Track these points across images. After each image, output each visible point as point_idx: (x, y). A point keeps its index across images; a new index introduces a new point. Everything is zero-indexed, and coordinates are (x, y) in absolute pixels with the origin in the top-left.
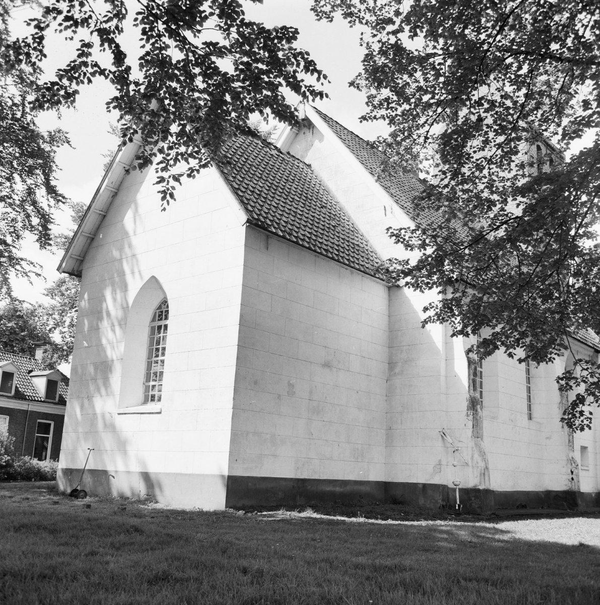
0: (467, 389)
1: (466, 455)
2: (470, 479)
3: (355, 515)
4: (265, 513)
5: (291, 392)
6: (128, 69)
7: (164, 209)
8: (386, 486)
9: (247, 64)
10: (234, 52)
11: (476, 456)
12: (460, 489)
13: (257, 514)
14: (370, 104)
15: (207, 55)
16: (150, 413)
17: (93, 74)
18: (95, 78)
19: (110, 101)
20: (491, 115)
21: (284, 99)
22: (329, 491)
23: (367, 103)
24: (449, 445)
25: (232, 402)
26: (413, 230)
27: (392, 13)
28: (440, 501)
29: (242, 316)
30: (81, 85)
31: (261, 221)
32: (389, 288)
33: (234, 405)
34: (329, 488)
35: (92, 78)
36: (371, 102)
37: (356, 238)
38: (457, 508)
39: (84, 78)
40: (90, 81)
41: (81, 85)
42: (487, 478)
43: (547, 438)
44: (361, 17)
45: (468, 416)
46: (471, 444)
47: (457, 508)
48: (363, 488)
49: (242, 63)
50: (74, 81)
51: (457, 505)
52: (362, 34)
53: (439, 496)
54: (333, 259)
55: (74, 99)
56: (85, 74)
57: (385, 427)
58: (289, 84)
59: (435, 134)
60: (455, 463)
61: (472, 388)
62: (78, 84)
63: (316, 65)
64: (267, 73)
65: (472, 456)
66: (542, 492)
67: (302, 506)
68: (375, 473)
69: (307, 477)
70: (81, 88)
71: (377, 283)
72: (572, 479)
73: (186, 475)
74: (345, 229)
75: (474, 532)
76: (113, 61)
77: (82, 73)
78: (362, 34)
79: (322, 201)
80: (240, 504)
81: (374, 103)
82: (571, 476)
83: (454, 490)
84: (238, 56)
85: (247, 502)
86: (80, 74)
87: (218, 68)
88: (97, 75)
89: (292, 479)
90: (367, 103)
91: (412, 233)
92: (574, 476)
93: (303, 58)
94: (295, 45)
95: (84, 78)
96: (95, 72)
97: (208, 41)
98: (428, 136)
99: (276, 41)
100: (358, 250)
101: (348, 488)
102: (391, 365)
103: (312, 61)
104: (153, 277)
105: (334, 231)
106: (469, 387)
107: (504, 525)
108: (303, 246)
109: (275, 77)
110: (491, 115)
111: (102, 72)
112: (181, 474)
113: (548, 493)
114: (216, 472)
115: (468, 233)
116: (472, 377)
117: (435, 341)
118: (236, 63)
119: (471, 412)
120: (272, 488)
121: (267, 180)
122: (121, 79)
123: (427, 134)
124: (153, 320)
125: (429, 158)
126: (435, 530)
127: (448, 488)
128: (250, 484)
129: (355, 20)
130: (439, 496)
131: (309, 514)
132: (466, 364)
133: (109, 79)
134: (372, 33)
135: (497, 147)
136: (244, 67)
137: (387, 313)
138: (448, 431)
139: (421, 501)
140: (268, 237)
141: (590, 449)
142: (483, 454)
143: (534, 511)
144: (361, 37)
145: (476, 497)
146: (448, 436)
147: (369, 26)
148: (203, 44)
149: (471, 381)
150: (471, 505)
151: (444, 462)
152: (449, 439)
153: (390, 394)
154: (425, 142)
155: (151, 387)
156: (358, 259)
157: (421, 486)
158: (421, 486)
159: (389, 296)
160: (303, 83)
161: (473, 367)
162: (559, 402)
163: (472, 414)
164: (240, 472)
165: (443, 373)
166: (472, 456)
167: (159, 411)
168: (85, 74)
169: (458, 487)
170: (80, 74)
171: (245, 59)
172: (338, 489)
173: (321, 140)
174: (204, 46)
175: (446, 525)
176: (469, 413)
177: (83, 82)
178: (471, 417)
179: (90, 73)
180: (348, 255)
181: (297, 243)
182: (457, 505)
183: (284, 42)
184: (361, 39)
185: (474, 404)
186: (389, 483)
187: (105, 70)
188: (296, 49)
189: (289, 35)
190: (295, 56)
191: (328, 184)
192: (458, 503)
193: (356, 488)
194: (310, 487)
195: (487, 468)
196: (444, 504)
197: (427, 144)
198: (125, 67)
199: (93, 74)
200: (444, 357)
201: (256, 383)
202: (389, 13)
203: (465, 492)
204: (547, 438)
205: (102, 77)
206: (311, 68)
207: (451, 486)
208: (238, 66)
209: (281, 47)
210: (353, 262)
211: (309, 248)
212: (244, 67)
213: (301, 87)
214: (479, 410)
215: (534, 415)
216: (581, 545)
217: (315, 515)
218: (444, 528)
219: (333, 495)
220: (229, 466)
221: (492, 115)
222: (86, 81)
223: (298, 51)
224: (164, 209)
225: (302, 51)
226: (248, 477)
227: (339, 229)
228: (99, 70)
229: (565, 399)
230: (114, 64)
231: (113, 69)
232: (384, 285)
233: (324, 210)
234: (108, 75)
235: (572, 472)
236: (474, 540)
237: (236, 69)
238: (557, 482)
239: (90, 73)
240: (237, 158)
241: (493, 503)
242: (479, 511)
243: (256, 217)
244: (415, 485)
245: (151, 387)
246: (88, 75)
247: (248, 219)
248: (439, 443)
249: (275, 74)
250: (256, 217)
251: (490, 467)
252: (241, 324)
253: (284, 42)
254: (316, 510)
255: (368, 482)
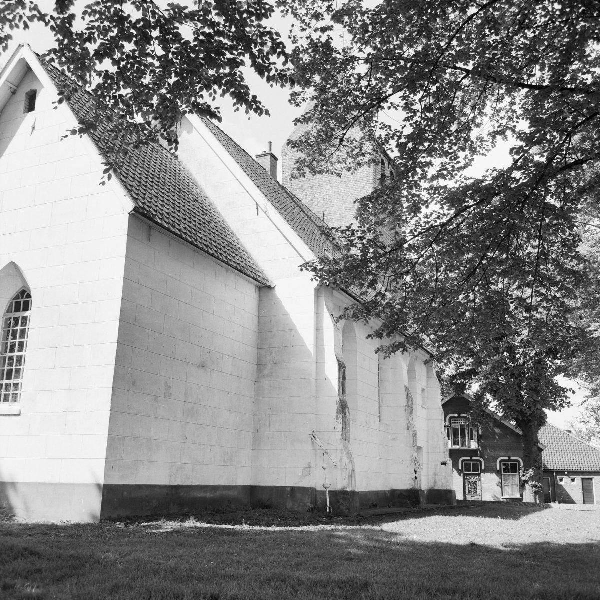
0: (338, 392)
1: (335, 457)
2: (339, 483)
3: (240, 524)
4: (145, 524)
5: (168, 395)
6: (72, 16)
7: (104, 183)
8: (252, 490)
9: (209, 36)
10: (196, 20)
11: (345, 458)
12: (330, 492)
13: (138, 525)
14: (293, 102)
15: (172, 19)
16: (9, 415)
17: (31, 18)
18: (32, 23)
19: (47, 52)
20: (411, 124)
21: (243, 79)
22: (200, 497)
23: (290, 101)
24: (319, 448)
25: (110, 404)
26: (344, 230)
27: (325, 8)
28: (309, 504)
29: (122, 311)
30: (15, 28)
31: (147, 210)
32: (260, 288)
33: (112, 407)
34: (200, 495)
35: (29, 23)
36: (294, 100)
37: (228, 235)
38: (328, 511)
39: (20, 21)
40: (26, 26)
41: (15, 28)
42: (353, 479)
43: (394, 439)
44: (295, 7)
45: (337, 418)
46: (341, 447)
47: (328, 511)
48: (231, 493)
49: (203, 33)
50: (8, 24)
51: (328, 508)
52: (293, 25)
53: (308, 499)
54: (213, 255)
55: (7, 44)
56: (21, 17)
57: (252, 430)
58: (255, 64)
59: (350, 137)
60: (325, 466)
61: (341, 391)
62: (12, 27)
63: (285, 47)
64: (231, 48)
65: (341, 459)
66: (388, 491)
67: (186, 515)
68: (244, 479)
69: (180, 484)
70: (15, 32)
71: (250, 282)
72: (416, 478)
73: (52, 484)
74: (217, 225)
75: (370, 536)
76: (55, 6)
77: (18, 15)
78: (293, 25)
79: (193, 194)
80: (115, 516)
81: (298, 101)
82: (415, 476)
83: (324, 493)
84: (200, 25)
85: (123, 513)
86: (15, 16)
87: (180, 35)
88: (36, 19)
89: (166, 486)
90: (290, 101)
91: (342, 233)
92: (417, 476)
93: (272, 38)
94: (264, 22)
95: (20, 21)
96: (33, 16)
97: (176, 3)
98: (344, 139)
99: (245, 15)
100: (232, 248)
101: (218, 494)
102: (260, 366)
103: (282, 43)
104: (13, 263)
105: (209, 226)
106: (339, 390)
107: (388, 527)
108: (186, 240)
109: (240, 54)
110: (411, 124)
111: (42, 17)
112: (45, 484)
113: (393, 492)
114: (91, 480)
115: (394, 237)
116: (342, 380)
117: (307, 343)
118: (197, 32)
119: (340, 415)
120: (147, 496)
121: (143, 167)
122: (63, 28)
123: (343, 137)
124: (9, 310)
125: (341, 160)
126: (333, 537)
127: (316, 491)
128: (126, 493)
129: (288, 9)
130: (308, 499)
131: (191, 523)
132: (337, 367)
133: (49, 27)
134: (301, 26)
135: (266, 162)
136: (204, 38)
137: (256, 313)
138: (317, 433)
139: (290, 505)
140: (150, 227)
141: (424, 450)
142: (350, 456)
143: (389, 510)
144: (291, 28)
145: (345, 499)
146: (318, 439)
147: (298, 19)
148: (169, 4)
149: (341, 385)
150: (339, 508)
151: (313, 465)
152: (319, 442)
153: (258, 397)
154: (341, 144)
155: (4, 387)
156: (234, 257)
157: (289, 490)
158: (289, 490)
159: (260, 296)
160: (275, 65)
161: (343, 370)
162: (405, 404)
163: (341, 417)
164: (117, 481)
165: (314, 375)
166: (341, 459)
167: (18, 413)
168: (21, 17)
169: (328, 490)
170: (15, 16)
171: (207, 30)
172: (209, 495)
173: (189, 132)
174: (169, 8)
175: (344, 530)
176: (339, 416)
177: (17, 26)
178: (341, 420)
179: (28, 17)
180: (225, 252)
181: (180, 236)
182: (328, 508)
183: (254, 18)
184: (291, 31)
185: (343, 407)
186: (256, 487)
187: (46, 15)
188: (265, 28)
189: (261, 12)
190: (262, 34)
191: (196, 178)
192: (329, 506)
193: (226, 493)
194: (182, 494)
195: (353, 470)
196: (313, 507)
197: (342, 146)
198: (68, 14)
199: (31, 18)
200: (315, 360)
201: (134, 383)
202: (321, 8)
203: (334, 494)
204: (394, 439)
205: (42, 23)
206: (278, 50)
207: (320, 488)
208: (199, 35)
209: (250, 23)
210: (231, 260)
211: (192, 243)
212: (204, 38)
213: (272, 69)
214: (347, 413)
215: (383, 418)
216: (473, 545)
217: (199, 525)
218: (339, 533)
219: (204, 501)
220: (105, 474)
221: (411, 125)
222: (22, 25)
223: (268, 29)
224: (104, 183)
225: (272, 30)
226: (124, 486)
227: (212, 225)
228: (38, 15)
229: (411, 402)
230: (56, 9)
231: (56, 15)
232: (256, 285)
233: (197, 204)
234: (49, 21)
235: (416, 472)
236: (371, 544)
237: (196, 39)
238: (403, 483)
239: (28, 17)
240: (105, 142)
241: (358, 505)
242: (347, 512)
243: (141, 205)
244: (283, 489)
245: (4, 387)
246: (25, 18)
247: (136, 207)
248: (309, 446)
249: (240, 51)
250: (141, 205)
251: (356, 469)
252: (122, 320)
253: (254, 18)
254: (199, 519)
255: (236, 487)
